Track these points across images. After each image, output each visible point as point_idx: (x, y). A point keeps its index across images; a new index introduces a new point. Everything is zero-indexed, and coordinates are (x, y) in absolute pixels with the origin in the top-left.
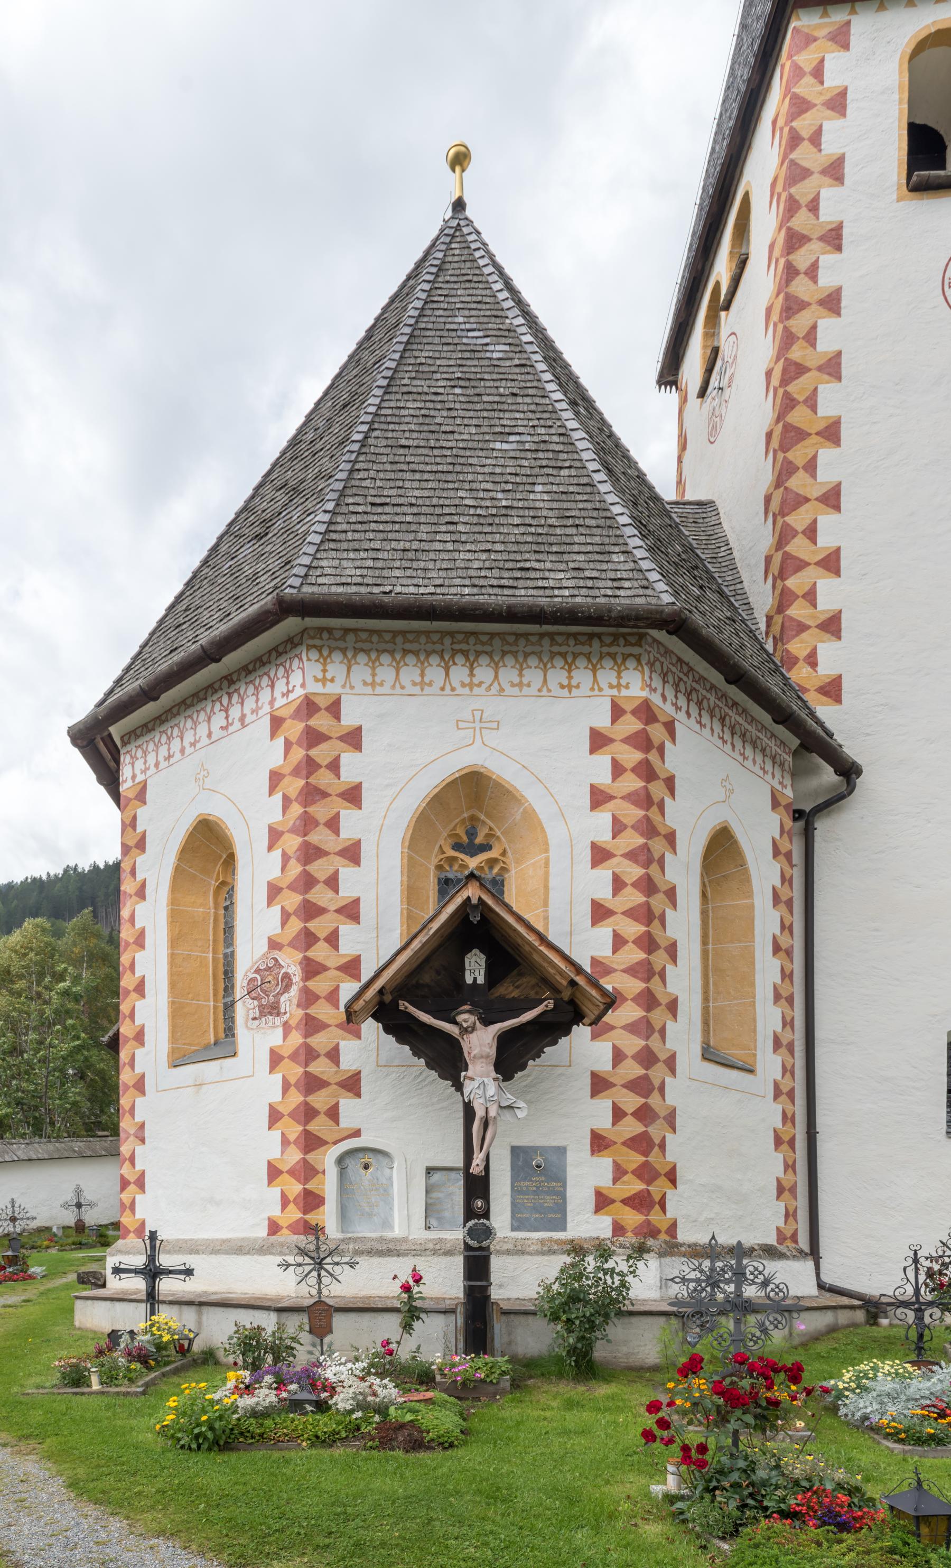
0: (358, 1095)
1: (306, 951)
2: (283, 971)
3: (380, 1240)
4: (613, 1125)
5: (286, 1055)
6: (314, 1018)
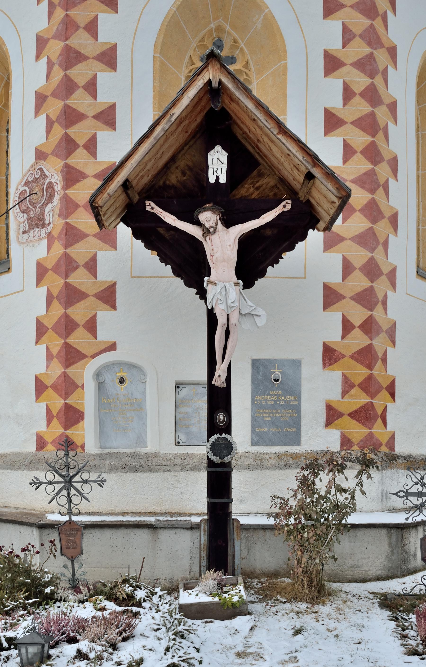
0: (114, 307)
1: (66, 160)
2: (48, 181)
3: (134, 455)
4: (343, 337)
5: (50, 267)
6: (73, 228)
